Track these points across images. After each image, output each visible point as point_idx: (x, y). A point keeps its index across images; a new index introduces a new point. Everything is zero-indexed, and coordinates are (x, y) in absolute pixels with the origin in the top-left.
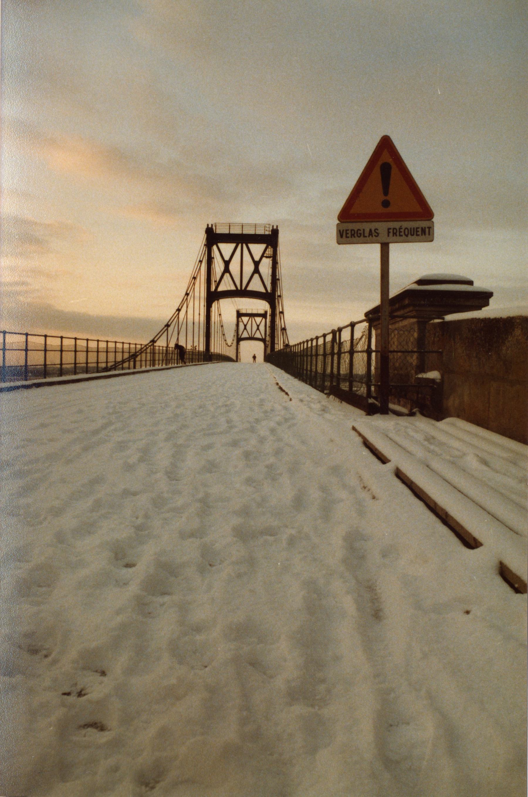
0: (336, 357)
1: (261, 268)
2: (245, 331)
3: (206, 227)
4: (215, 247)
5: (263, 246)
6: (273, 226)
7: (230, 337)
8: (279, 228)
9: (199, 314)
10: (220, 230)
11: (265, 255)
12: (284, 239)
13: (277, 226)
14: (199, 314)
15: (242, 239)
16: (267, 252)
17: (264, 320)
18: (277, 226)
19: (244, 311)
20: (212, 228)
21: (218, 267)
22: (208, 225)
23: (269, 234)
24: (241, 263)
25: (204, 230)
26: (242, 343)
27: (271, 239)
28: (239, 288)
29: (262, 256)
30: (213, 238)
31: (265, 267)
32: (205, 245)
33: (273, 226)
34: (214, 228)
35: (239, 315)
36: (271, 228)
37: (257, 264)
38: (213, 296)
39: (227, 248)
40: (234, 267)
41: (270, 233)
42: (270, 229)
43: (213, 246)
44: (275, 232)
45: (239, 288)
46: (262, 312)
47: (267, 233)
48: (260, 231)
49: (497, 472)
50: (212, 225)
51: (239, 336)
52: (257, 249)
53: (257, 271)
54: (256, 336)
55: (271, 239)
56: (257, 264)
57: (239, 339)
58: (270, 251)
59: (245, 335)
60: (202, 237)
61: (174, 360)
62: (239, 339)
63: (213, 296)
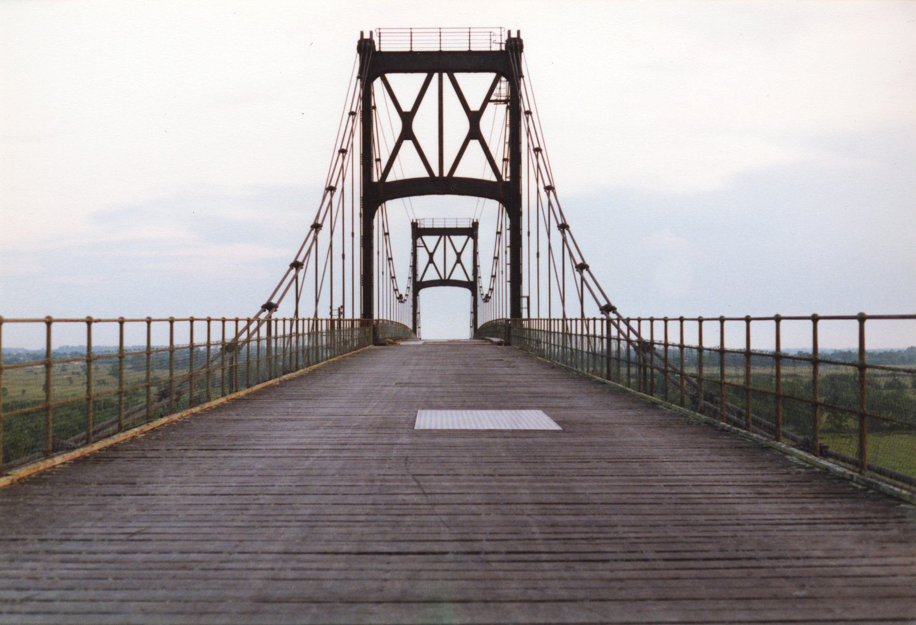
0: (273, 334)
1: (485, 125)
2: (431, 265)
3: (359, 38)
4: (378, 84)
5: (488, 78)
6: (509, 32)
7: (404, 284)
8: (522, 37)
9: (353, 234)
10: (388, 44)
11: (493, 98)
12: (529, 61)
13: (519, 32)
14: (353, 234)
15: (439, 64)
16: (496, 91)
17: (471, 241)
18: (519, 32)
19: (428, 225)
20: (371, 41)
21: (387, 126)
22: (362, 33)
23: (501, 51)
24: (442, 124)
25: (356, 44)
26: (424, 293)
27: (506, 61)
28: (437, 174)
29: (487, 100)
30: (375, 62)
31: (495, 123)
32: (358, 78)
33: (509, 32)
34: (376, 39)
35: (418, 232)
36: (505, 38)
37: (474, 118)
38: (376, 193)
39: (406, 84)
40: (424, 126)
41: (503, 48)
42: (504, 41)
43: (374, 79)
44: (515, 46)
45: (437, 174)
46: (467, 225)
47: (496, 48)
48: (481, 45)
49: (139, 589)
50: (371, 33)
51: (418, 279)
52: (476, 84)
53: (475, 133)
54: (453, 278)
55: (506, 61)
56: (474, 118)
57: (418, 286)
58: (503, 88)
59: (432, 275)
60: (352, 62)
61: (303, 334)
62: (418, 286)
63: (376, 193)
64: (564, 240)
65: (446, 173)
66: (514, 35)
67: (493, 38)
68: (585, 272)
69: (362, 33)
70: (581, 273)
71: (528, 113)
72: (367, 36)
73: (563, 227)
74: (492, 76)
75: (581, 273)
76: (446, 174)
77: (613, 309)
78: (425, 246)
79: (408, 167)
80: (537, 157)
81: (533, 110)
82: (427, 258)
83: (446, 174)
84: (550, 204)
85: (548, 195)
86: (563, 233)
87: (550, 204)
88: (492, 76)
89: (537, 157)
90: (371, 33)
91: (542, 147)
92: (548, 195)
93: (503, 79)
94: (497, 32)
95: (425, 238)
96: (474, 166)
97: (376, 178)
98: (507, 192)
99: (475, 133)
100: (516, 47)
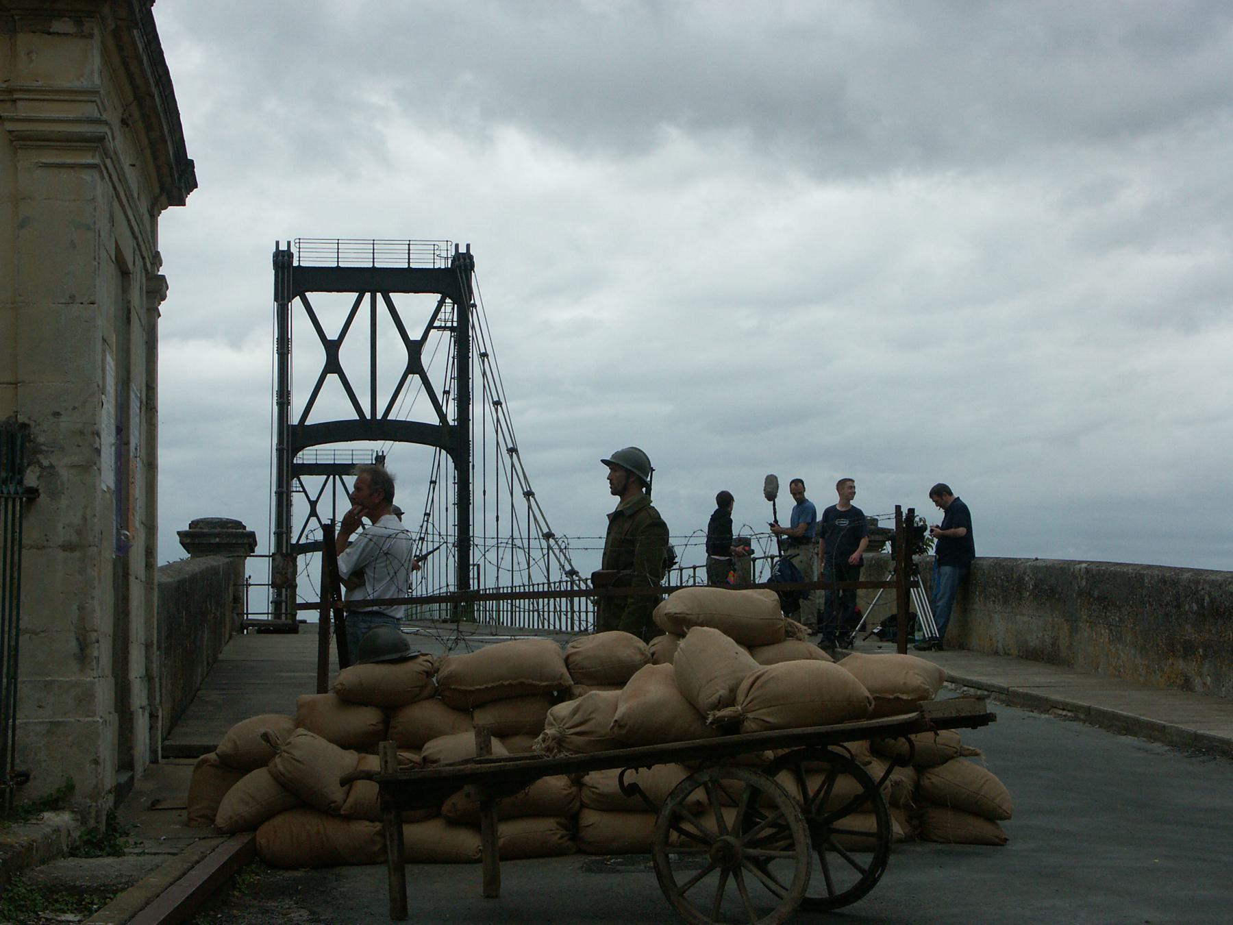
6: (457, 246)
10: (306, 258)
11: (437, 324)
13: (468, 246)
18: (468, 246)
22: (277, 243)
23: (446, 269)
27: (453, 280)
29: (430, 326)
31: (438, 355)
33: (457, 246)
34: (294, 250)
37: (415, 349)
39: (332, 307)
44: (463, 264)
45: (368, 417)
47: (440, 264)
50: (289, 243)
52: (417, 307)
53: (415, 366)
55: (453, 280)
56: (415, 349)
64: (530, 507)
65: (379, 416)
66: (463, 250)
67: (437, 252)
68: (551, 541)
69: (277, 243)
70: (548, 541)
71: (484, 355)
72: (283, 247)
73: (529, 494)
74: (438, 296)
75: (548, 541)
76: (379, 417)
77: (576, 573)
78: (304, 491)
79: (333, 406)
80: (497, 410)
81: (489, 352)
82: (307, 509)
83: (379, 417)
84: (513, 465)
85: (511, 457)
86: (528, 500)
87: (513, 465)
88: (438, 296)
89: (497, 410)
90: (289, 243)
91: (502, 400)
92: (511, 457)
93: (448, 300)
94: (443, 246)
95: (305, 478)
96: (416, 407)
97: (295, 419)
98: (453, 439)
99: (415, 366)
100: (465, 266)
